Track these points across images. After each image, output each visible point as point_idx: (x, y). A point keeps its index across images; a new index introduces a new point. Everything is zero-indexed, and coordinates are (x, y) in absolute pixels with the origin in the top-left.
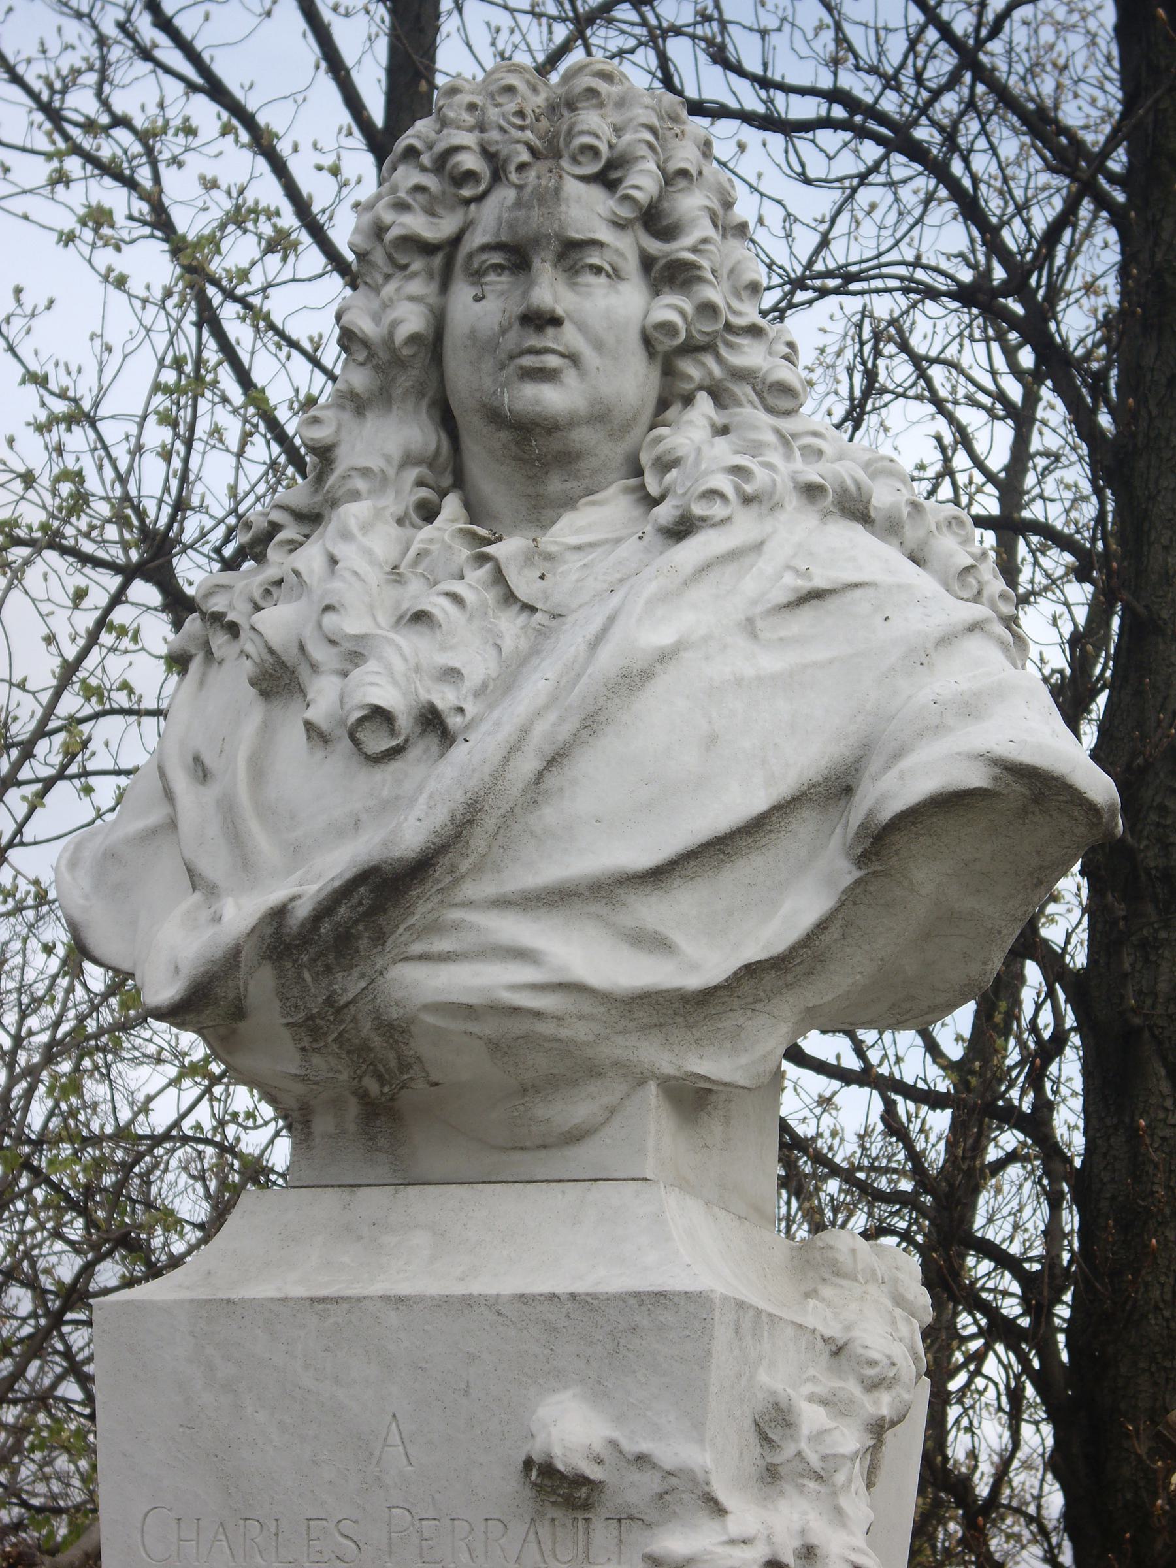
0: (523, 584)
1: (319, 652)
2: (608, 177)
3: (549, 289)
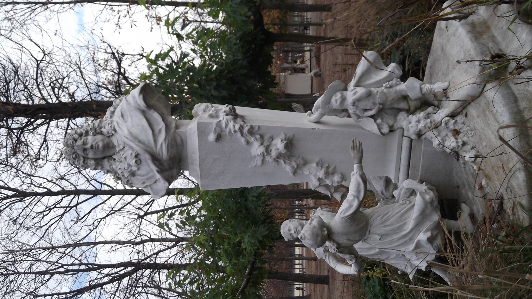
0: (121, 147)
1: (129, 170)
2: (76, 140)
3: (89, 146)
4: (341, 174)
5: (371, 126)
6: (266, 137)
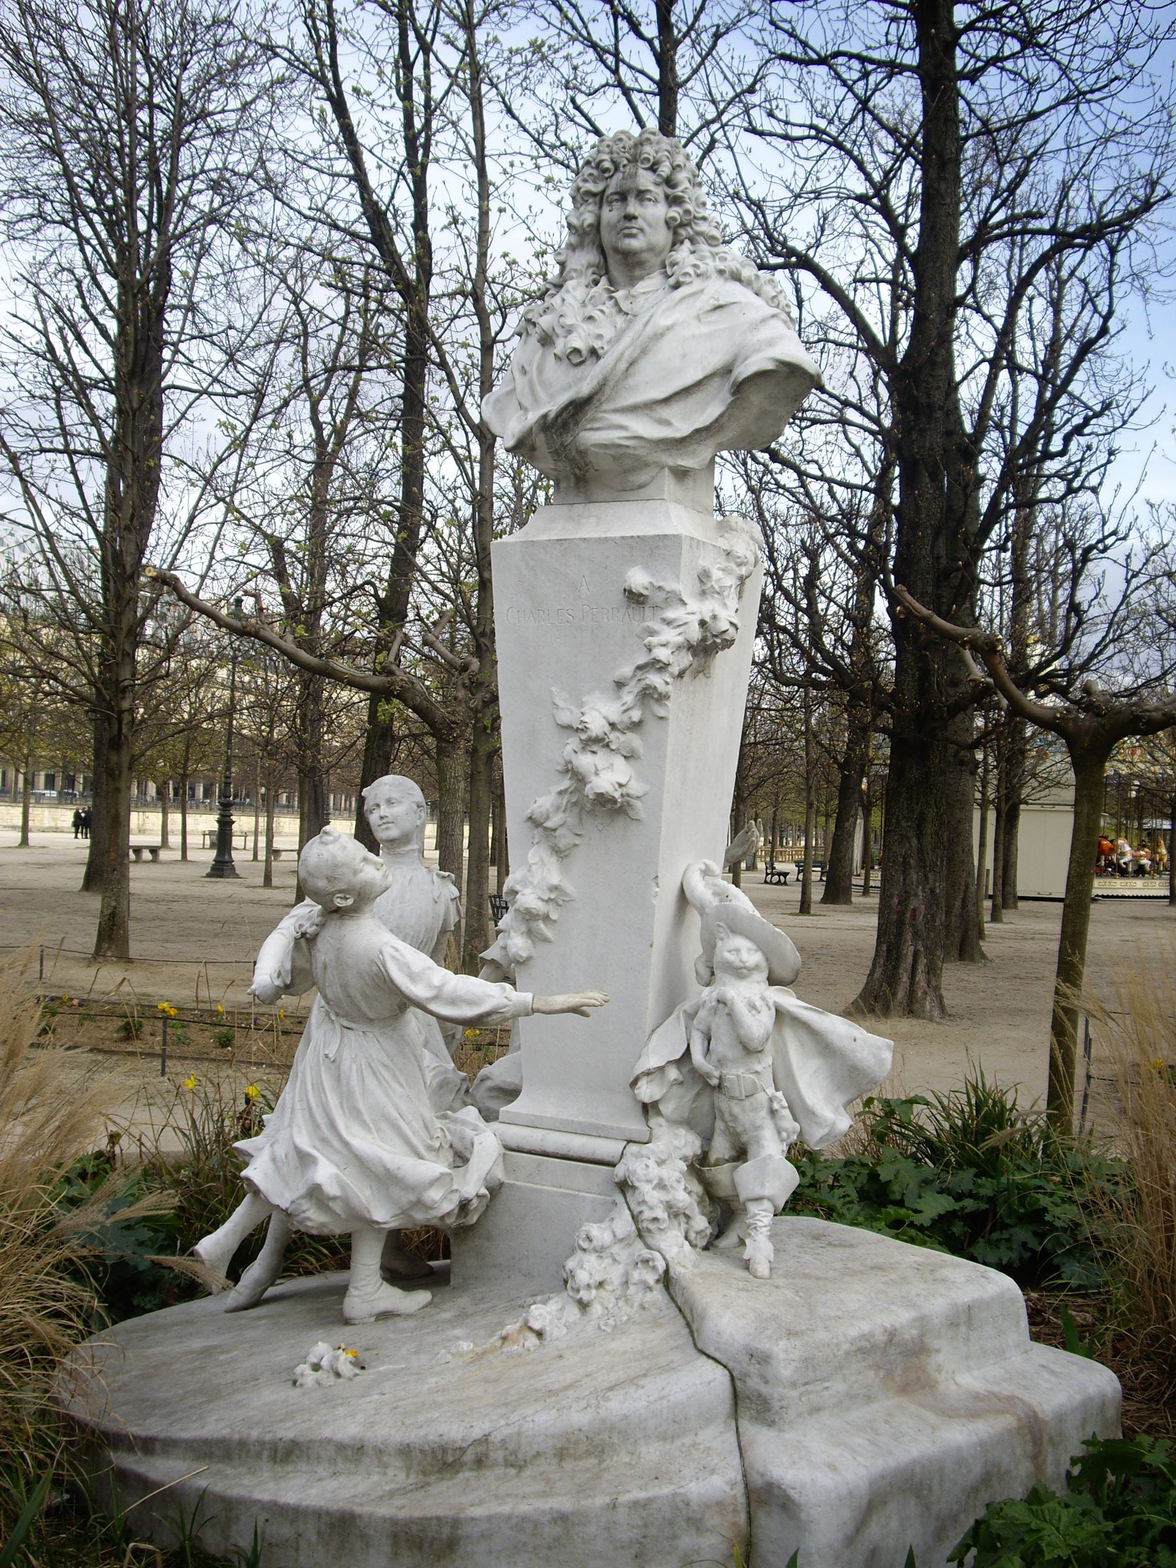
0: (625, 306)
1: (559, 331)
2: (653, 168)
3: (633, 207)
4: (529, 958)
5: (660, 1050)
6: (633, 740)
